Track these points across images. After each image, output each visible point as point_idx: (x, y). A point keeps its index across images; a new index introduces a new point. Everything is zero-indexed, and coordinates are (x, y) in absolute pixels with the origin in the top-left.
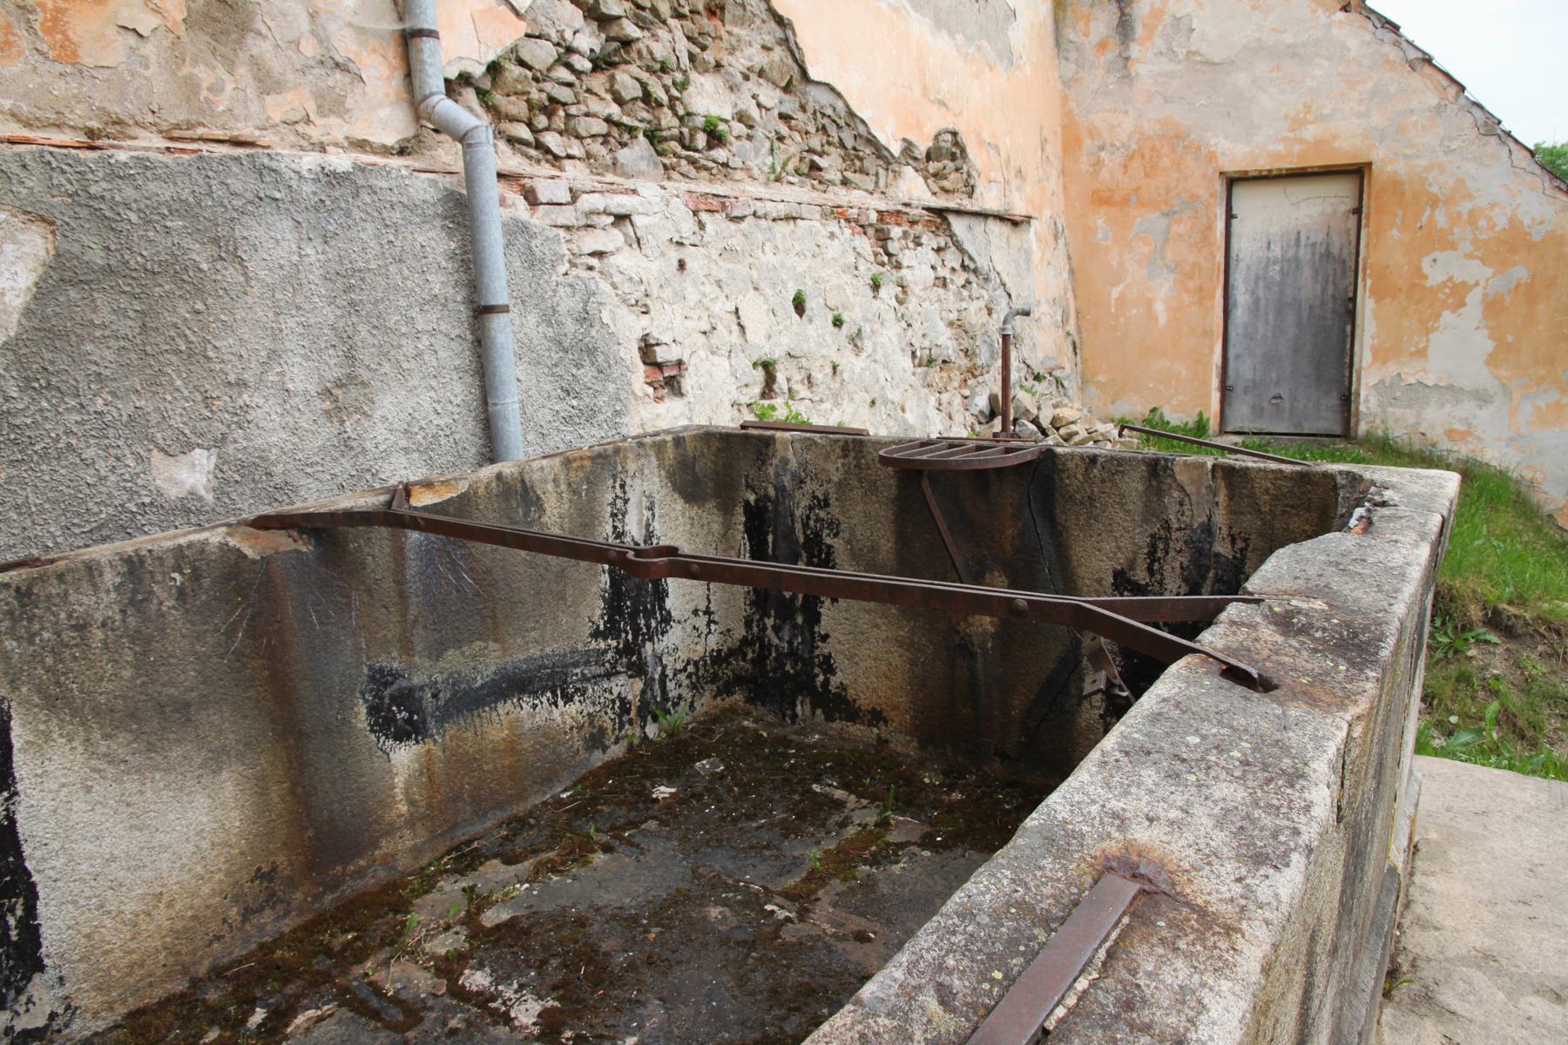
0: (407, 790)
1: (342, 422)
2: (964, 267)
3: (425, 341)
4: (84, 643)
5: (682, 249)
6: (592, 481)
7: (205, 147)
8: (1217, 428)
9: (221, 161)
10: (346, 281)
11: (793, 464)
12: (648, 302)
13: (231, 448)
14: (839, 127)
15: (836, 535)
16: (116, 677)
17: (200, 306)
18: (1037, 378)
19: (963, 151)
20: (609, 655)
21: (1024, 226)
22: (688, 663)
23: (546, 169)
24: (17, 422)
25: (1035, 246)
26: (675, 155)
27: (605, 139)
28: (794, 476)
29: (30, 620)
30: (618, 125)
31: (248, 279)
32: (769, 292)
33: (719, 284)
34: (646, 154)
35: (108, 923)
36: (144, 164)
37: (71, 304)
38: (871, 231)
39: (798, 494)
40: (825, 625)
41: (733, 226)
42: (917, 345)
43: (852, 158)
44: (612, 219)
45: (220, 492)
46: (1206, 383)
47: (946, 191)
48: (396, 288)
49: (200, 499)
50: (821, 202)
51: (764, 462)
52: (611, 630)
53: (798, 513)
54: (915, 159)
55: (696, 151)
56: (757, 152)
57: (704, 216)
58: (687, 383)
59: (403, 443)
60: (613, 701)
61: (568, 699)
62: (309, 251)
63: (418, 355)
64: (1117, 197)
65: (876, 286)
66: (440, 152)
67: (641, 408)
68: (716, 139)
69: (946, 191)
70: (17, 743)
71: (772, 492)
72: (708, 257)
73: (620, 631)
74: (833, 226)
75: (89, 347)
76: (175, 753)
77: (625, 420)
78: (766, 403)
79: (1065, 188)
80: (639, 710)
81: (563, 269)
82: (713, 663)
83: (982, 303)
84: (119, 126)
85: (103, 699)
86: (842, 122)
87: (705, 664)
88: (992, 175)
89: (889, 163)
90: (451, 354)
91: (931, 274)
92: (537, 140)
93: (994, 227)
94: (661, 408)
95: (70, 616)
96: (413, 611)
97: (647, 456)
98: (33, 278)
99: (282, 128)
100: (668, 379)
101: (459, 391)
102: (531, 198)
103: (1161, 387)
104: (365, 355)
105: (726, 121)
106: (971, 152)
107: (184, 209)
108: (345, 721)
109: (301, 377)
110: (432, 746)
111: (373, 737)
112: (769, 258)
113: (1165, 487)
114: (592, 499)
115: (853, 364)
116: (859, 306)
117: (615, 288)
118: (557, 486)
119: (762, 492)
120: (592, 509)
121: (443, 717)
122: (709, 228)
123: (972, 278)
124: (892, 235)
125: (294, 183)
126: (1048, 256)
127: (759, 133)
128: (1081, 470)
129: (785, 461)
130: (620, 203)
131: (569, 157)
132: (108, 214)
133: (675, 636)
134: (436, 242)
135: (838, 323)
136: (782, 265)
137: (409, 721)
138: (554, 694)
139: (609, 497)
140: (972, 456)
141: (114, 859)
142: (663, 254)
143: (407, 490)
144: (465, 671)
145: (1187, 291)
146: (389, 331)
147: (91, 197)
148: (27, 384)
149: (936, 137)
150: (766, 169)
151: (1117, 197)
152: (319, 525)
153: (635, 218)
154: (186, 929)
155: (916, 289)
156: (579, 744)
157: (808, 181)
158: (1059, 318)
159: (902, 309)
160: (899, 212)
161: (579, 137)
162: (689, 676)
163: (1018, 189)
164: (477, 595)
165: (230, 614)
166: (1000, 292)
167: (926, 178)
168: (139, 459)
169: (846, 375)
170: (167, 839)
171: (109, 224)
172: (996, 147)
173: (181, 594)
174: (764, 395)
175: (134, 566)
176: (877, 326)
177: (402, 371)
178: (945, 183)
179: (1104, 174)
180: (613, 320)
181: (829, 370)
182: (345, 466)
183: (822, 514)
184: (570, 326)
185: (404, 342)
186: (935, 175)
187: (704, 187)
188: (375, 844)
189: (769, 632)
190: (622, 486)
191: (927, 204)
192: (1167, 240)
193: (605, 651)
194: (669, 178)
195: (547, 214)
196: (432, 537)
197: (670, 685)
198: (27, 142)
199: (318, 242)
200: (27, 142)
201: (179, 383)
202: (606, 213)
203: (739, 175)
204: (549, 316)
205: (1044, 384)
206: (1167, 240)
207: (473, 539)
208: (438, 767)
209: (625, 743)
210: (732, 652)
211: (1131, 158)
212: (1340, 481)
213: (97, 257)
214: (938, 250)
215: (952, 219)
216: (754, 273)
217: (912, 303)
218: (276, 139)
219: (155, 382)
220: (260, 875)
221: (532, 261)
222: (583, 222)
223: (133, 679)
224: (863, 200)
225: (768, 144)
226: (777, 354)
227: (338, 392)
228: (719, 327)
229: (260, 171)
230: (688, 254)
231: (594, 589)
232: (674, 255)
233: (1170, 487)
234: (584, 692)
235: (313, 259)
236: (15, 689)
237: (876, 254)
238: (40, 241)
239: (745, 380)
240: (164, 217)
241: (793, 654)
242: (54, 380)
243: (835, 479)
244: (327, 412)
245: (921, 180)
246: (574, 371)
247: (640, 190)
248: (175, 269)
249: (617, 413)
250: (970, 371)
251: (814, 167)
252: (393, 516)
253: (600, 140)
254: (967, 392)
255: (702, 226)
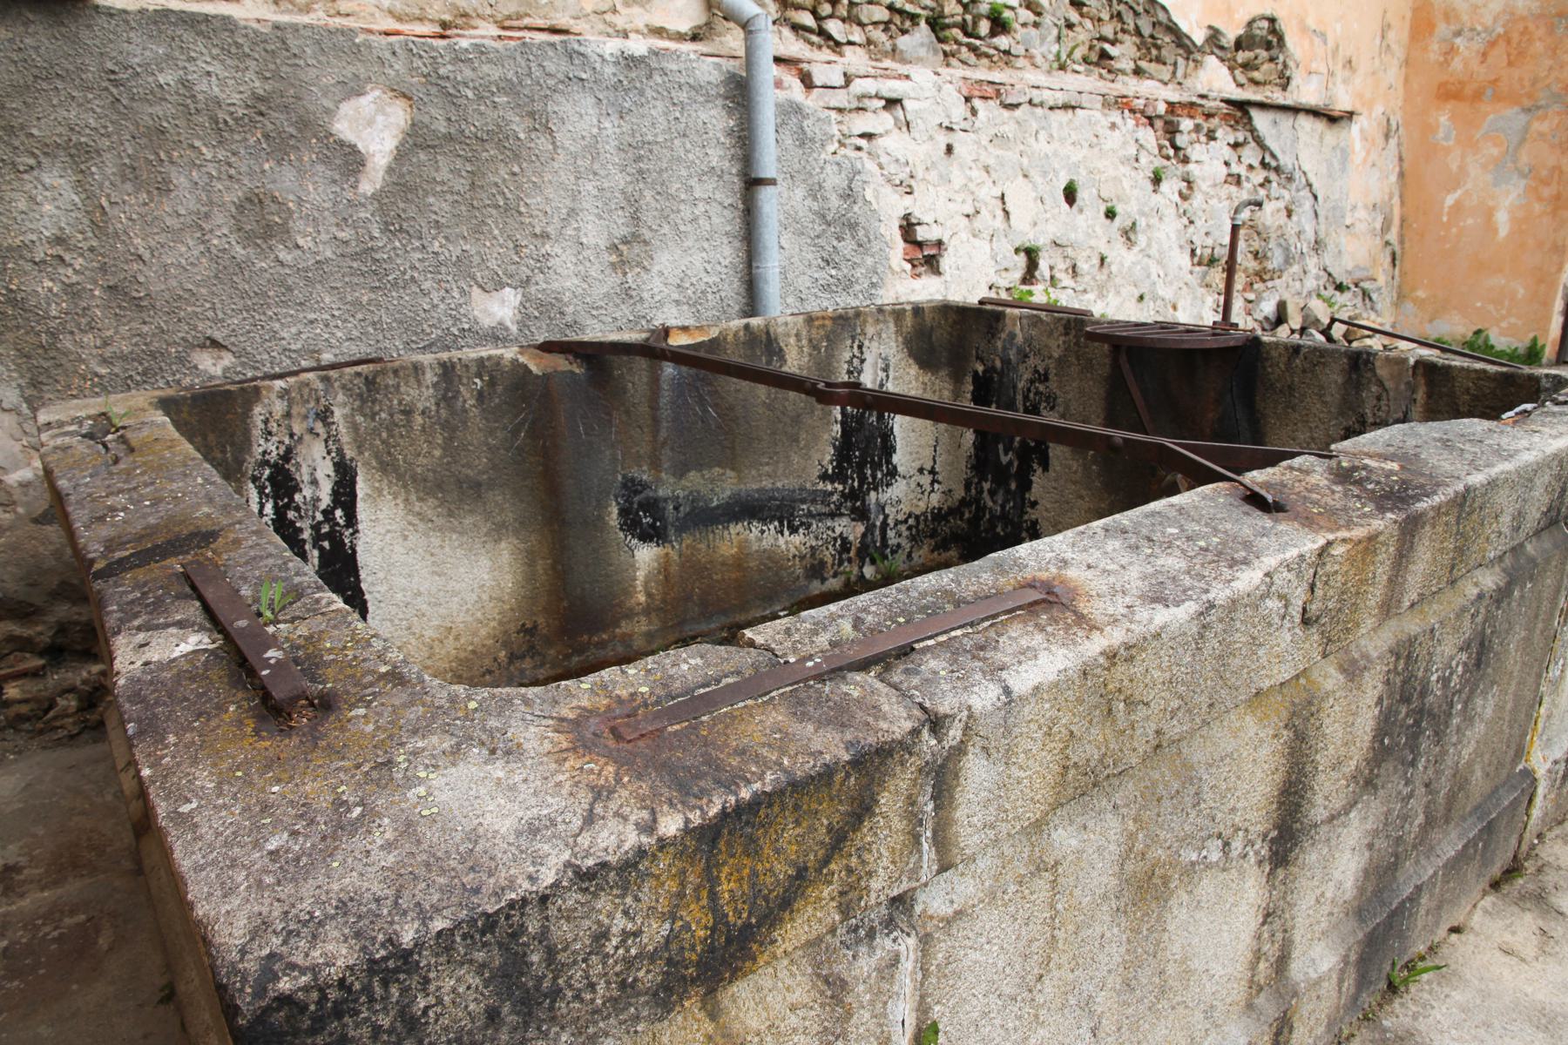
0: (646, 583)
1: (625, 274)
2: (1264, 165)
3: (701, 207)
4: (409, 424)
5: (951, 134)
6: (832, 339)
7: (527, 34)
8: (1553, 357)
9: (540, 47)
10: (636, 152)
11: (1020, 338)
12: (913, 182)
13: (533, 289)
14: (1136, 14)
15: (1052, 408)
16: (428, 455)
17: (516, 169)
18: (1340, 288)
19: (1281, 39)
20: (835, 498)
21: (1344, 123)
22: (910, 516)
23: (826, 54)
24: (377, 257)
25: (1358, 145)
26: (957, 42)
27: (886, 26)
28: (1020, 351)
29: (374, 402)
30: (901, 12)
31: (555, 147)
32: (1038, 179)
33: (987, 169)
34: (926, 41)
35: (413, 641)
36: (480, 50)
37: (420, 165)
38: (1159, 124)
39: (1021, 368)
40: (1036, 492)
41: (1006, 113)
42: (1198, 243)
43: (1149, 47)
44: (883, 103)
45: (522, 325)
46: (1547, 304)
47: (1256, 83)
48: (679, 159)
49: (507, 329)
50: (1104, 91)
51: (993, 336)
52: (838, 476)
53: (1020, 385)
54: (1222, 48)
55: (979, 38)
56: (1043, 39)
57: (977, 103)
58: (945, 263)
59: (676, 296)
60: (835, 539)
61: (794, 530)
62: (607, 125)
63: (695, 220)
64: (1468, 91)
65: (1157, 180)
66: (729, 38)
67: (897, 282)
68: (999, 25)
69: (1256, 83)
70: (360, 494)
71: (998, 364)
72: (978, 143)
73: (847, 477)
74: (1115, 116)
75: (431, 200)
76: (468, 521)
77: (880, 292)
78: (1025, 288)
79: (1406, 80)
80: (859, 551)
81: (832, 147)
82: (934, 519)
83: (1281, 204)
84: (465, 17)
85: (419, 470)
86: (1140, 9)
87: (926, 520)
88: (1314, 66)
89: (1189, 52)
90: (722, 219)
91: (1224, 170)
92: (820, 27)
93: (1305, 122)
94: (917, 284)
95: (400, 403)
96: (663, 434)
97: (885, 322)
98: (395, 143)
99: (593, 17)
100: (927, 257)
101: (727, 254)
102: (807, 81)
103: (1491, 307)
104: (648, 217)
105: (1012, 8)
106: (1290, 41)
107: (509, 88)
108: (600, 518)
109: (594, 232)
110: (672, 551)
111: (621, 535)
112: (1041, 146)
113: (1364, 381)
114: (830, 356)
115: (1121, 256)
116: (1134, 197)
117: (881, 168)
118: (799, 340)
119: (989, 364)
120: (830, 364)
121: (682, 528)
122: (981, 114)
123: (1273, 176)
124: (1182, 127)
125: (598, 66)
126: (1373, 156)
127: (1047, 20)
128: (1284, 359)
129: (1012, 336)
130: (892, 88)
131: (850, 43)
132: (451, 91)
133: (898, 490)
134: (716, 120)
135: (1110, 214)
136: (1056, 154)
137: (653, 526)
138: (781, 524)
139: (847, 355)
140: (1186, 337)
141: (419, 594)
142: (931, 138)
143: (666, 332)
144: (704, 491)
145: (1540, 199)
146: (670, 197)
147: (440, 77)
148: (386, 228)
149: (1250, 24)
150: (1051, 57)
151: (1468, 91)
152: (589, 351)
153: (906, 103)
154: (467, 660)
155: (1203, 185)
156: (799, 571)
157: (1097, 70)
158: (1378, 226)
159: (1186, 205)
160: (1192, 104)
161: (861, 24)
162: (910, 528)
163: (1345, 81)
164: (719, 427)
165: (516, 416)
166: (1305, 193)
167: (1231, 69)
168: (463, 292)
169: (1114, 268)
170: (458, 587)
171: (451, 99)
172: (1323, 36)
173: (480, 396)
174: (1024, 281)
175: (447, 369)
176: (1154, 221)
177: (679, 233)
178: (1256, 75)
179: (1457, 64)
180: (877, 198)
181: (1096, 261)
182: (625, 311)
183: (1041, 388)
184: (835, 202)
185: (682, 207)
186: (1246, 66)
187: (982, 73)
188: (616, 624)
189: (985, 495)
190: (860, 347)
191: (1226, 96)
192: (1523, 140)
193: (831, 494)
194: (948, 65)
195: (820, 97)
196: (684, 369)
197: (891, 534)
198: (397, 33)
199: (615, 117)
200: (397, 33)
201: (496, 232)
202: (877, 96)
203: (1021, 62)
204: (815, 192)
205: (1348, 295)
206: (1523, 140)
207: (723, 377)
208: (674, 569)
209: (843, 578)
210: (951, 511)
211: (1493, 44)
212: (1545, 383)
213: (441, 127)
214: (1236, 146)
215: (1255, 114)
216: (1025, 161)
217: (1197, 200)
218: (587, 27)
219: (478, 230)
220: (523, 630)
221: (803, 140)
222: (855, 104)
223: (441, 458)
224: (1156, 92)
225: (1055, 32)
226: (1040, 239)
227: (622, 247)
228: (983, 211)
229: (571, 55)
230: (957, 139)
231: (826, 436)
232: (943, 139)
233: (1370, 381)
234: (808, 526)
235: (610, 132)
236: (361, 453)
237: (1161, 148)
238: (401, 113)
239: (1005, 264)
240: (493, 94)
241: (1004, 517)
242: (405, 225)
243: (1056, 355)
244: (613, 264)
245: (1225, 71)
246: (835, 243)
247: (913, 76)
248: (499, 137)
249: (873, 285)
250: (1257, 274)
251: (1104, 55)
252: (653, 350)
253: (882, 27)
254: (1251, 296)
255: (974, 112)
